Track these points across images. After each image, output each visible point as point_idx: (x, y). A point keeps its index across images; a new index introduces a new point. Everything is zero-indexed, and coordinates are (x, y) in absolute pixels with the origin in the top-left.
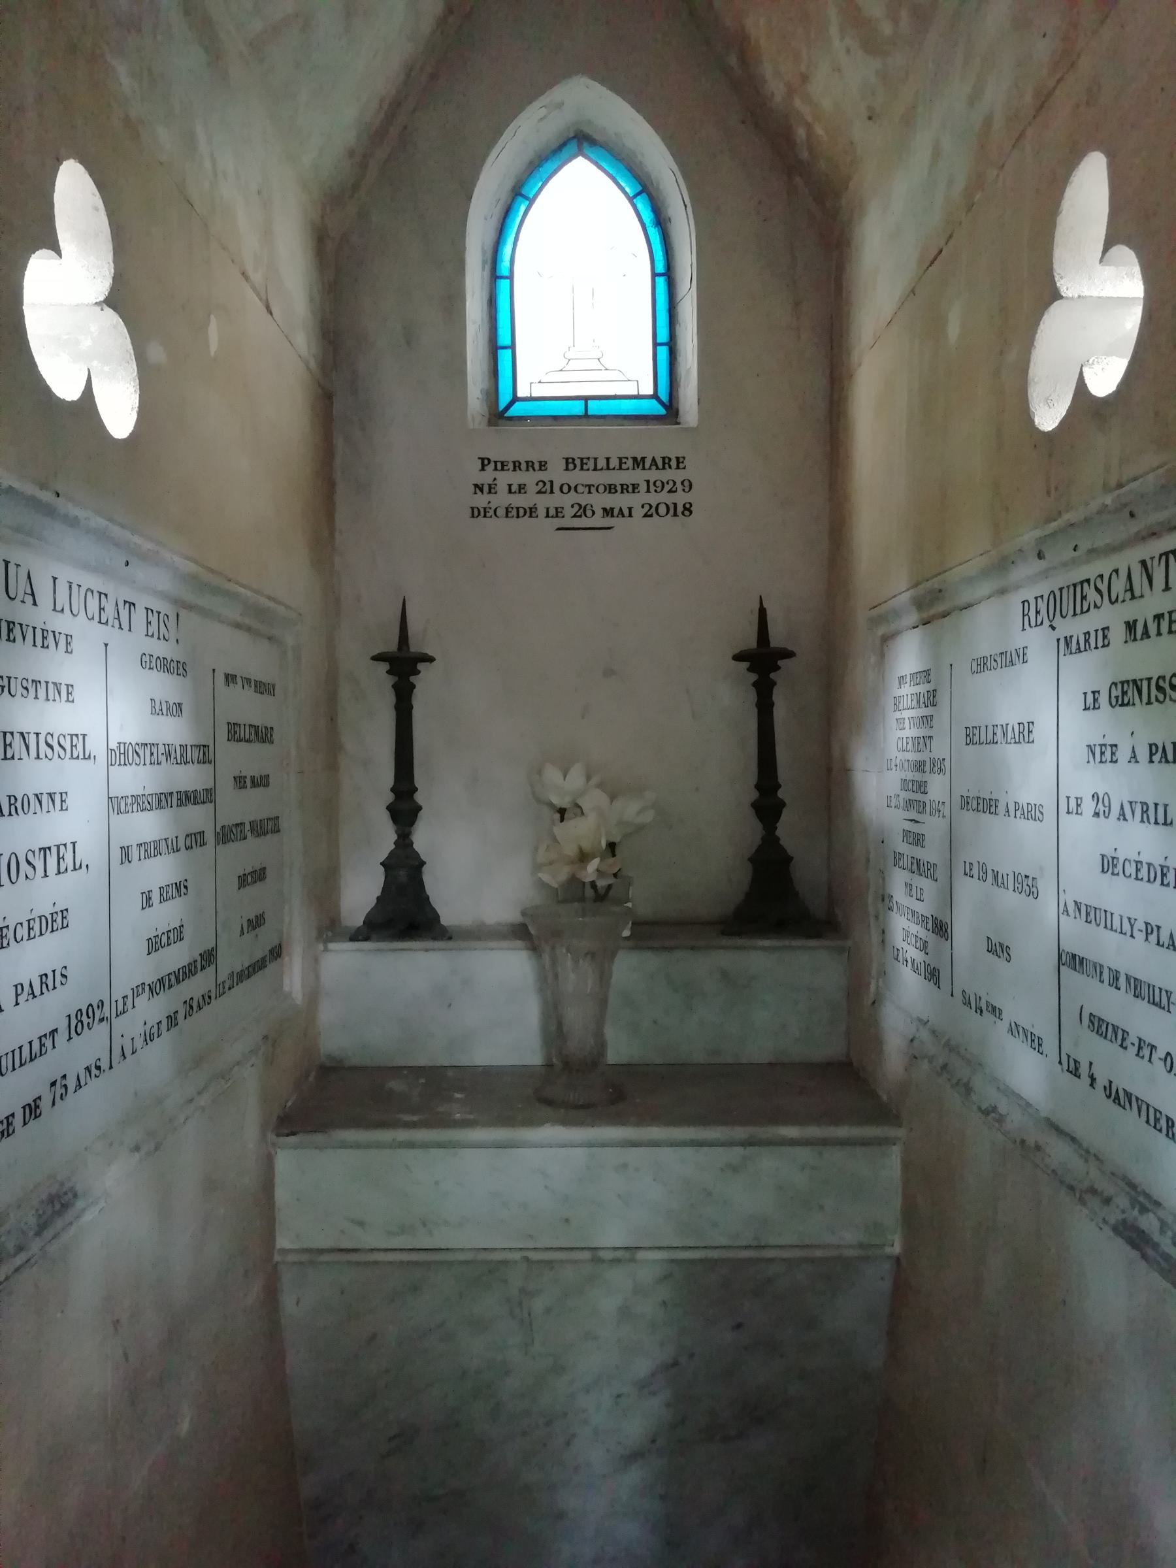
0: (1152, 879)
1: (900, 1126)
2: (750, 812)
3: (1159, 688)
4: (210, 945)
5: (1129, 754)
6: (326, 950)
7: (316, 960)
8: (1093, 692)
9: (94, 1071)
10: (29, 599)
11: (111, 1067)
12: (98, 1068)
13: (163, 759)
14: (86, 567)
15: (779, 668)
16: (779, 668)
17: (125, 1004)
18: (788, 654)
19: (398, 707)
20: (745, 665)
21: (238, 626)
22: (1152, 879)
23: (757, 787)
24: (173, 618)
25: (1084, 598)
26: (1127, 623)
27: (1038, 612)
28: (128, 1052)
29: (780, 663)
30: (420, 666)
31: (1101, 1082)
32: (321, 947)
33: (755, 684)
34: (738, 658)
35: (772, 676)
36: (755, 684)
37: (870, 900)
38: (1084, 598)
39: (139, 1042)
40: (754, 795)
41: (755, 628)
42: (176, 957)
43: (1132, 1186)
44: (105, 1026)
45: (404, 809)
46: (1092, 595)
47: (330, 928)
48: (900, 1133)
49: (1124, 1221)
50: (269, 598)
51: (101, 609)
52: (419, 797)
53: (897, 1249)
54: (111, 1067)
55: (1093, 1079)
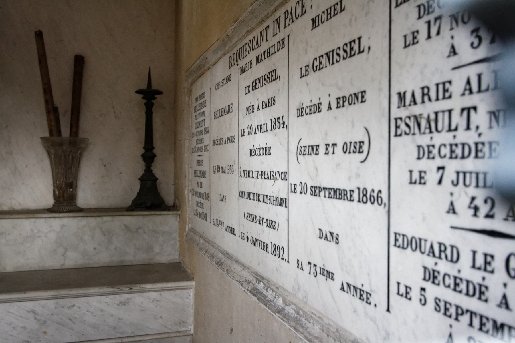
1: (193, 280)
2: (141, 159)
3: (265, 79)
5: (257, 107)
8: (294, 185)
15: (155, 98)
16: (155, 98)
18: (160, 93)
20: (142, 96)
23: (144, 148)
25: (246, 50)
26: (257, 57)
27: (234, 60)
29: (156, 96)
31: (250, 238)
33: (145, 104)
34: (138, 92)
35: (153, 101)
36: (145, 104)
37: (186, 192)
38: (246, 50)
40: (143, 151)
41: (147, 79)
43: (257, 274)
46: (248, 49)
48: (193, 283)
49: (253, 288)
53: (192, 332)
55: (248, 238)
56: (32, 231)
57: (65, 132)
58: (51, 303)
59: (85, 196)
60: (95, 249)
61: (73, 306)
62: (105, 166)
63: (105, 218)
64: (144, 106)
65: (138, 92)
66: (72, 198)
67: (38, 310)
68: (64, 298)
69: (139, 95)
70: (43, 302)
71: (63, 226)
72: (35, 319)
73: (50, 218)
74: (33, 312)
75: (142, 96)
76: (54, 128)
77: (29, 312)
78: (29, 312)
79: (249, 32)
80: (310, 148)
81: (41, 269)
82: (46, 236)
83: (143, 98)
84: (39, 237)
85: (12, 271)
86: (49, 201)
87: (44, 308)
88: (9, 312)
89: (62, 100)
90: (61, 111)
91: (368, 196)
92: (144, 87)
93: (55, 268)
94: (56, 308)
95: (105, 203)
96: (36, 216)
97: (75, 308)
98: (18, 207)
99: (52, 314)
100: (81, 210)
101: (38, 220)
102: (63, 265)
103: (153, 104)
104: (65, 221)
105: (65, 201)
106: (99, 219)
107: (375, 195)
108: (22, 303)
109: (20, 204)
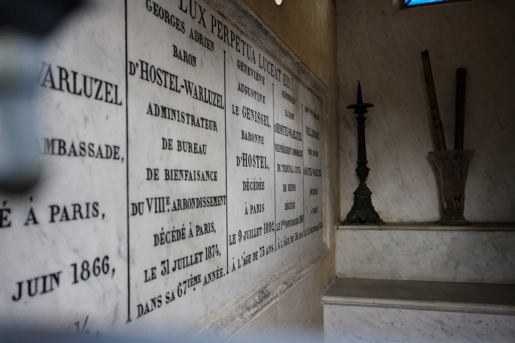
0: (157, 114)
4: (302, 214)
6: (338, 229)
7: (334, 232)
9: (157, 303)
10: (253, 60)
11: (228, 273)
12: (160, 301)
13: (288, 134)
14: (268, 52)
15: (367, 112)
17: (234, 239)
19: (359, 128)
20: (353, 110)
21: (309, 89)
22: (157, 114)
24: (291, 80)
28: (236, 266)
30: (367, 109)
32: (336, 227)
34: (349, 107)
39: (242, 262)
42: (292, 214)
44: (273, 232)
45: (363, 171)
47: (338, 222)
50: (319, 79)
51: (272, 70)
52: (369, 165)
54: (228, 273)
56: (424, 242)
57: (450, 146)
58: (458, 316)
59: (471, 210)
60: (487, 264)
61: (481, 322)
62: (491, 178)
63: (498, 233)
64: (356, 121)
65: (349, 107)
66: (460, 210)
67: (445, 321)
68: (470, 312)
69: (350, 109)
70: (450, 314)
71: (453, 240)
72: (443, 329)
73: (441, 230)
74: (441, 322)
75: (353, 110)
76: (439, 144)
77: (436, 321)
78: (436, 321)
79: (235, 26)
80: (193, 178)
81: (434, 280)
82: (437, 248)
83: (355, 112)
84: (431, 249)
85: (407, 279)
86: (435, 214)
87: (451, 319)
88: (418, 319)
89: (447, 116)
90: (444, 125)
91: (91, 268)
92: (354, 102)
93: (439, 281)
94: (462, 321)
95: (492, 218)
96: (428, 228)
97: (483, 324)
98: (406, 220)
99: (459, 327)
100: (469, 224)
101: (430, 232)
102: (455, 278)
103: (365, 118)
104: (455, 234)
105: (451, 214)
106: (491, 234)
107: (100, 264)
108: (429, 312)
109: (407, 216)
